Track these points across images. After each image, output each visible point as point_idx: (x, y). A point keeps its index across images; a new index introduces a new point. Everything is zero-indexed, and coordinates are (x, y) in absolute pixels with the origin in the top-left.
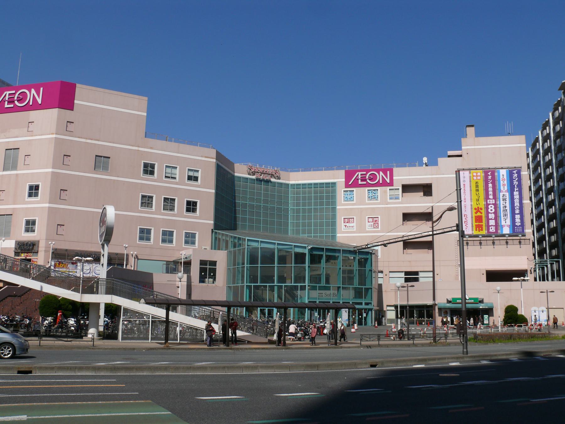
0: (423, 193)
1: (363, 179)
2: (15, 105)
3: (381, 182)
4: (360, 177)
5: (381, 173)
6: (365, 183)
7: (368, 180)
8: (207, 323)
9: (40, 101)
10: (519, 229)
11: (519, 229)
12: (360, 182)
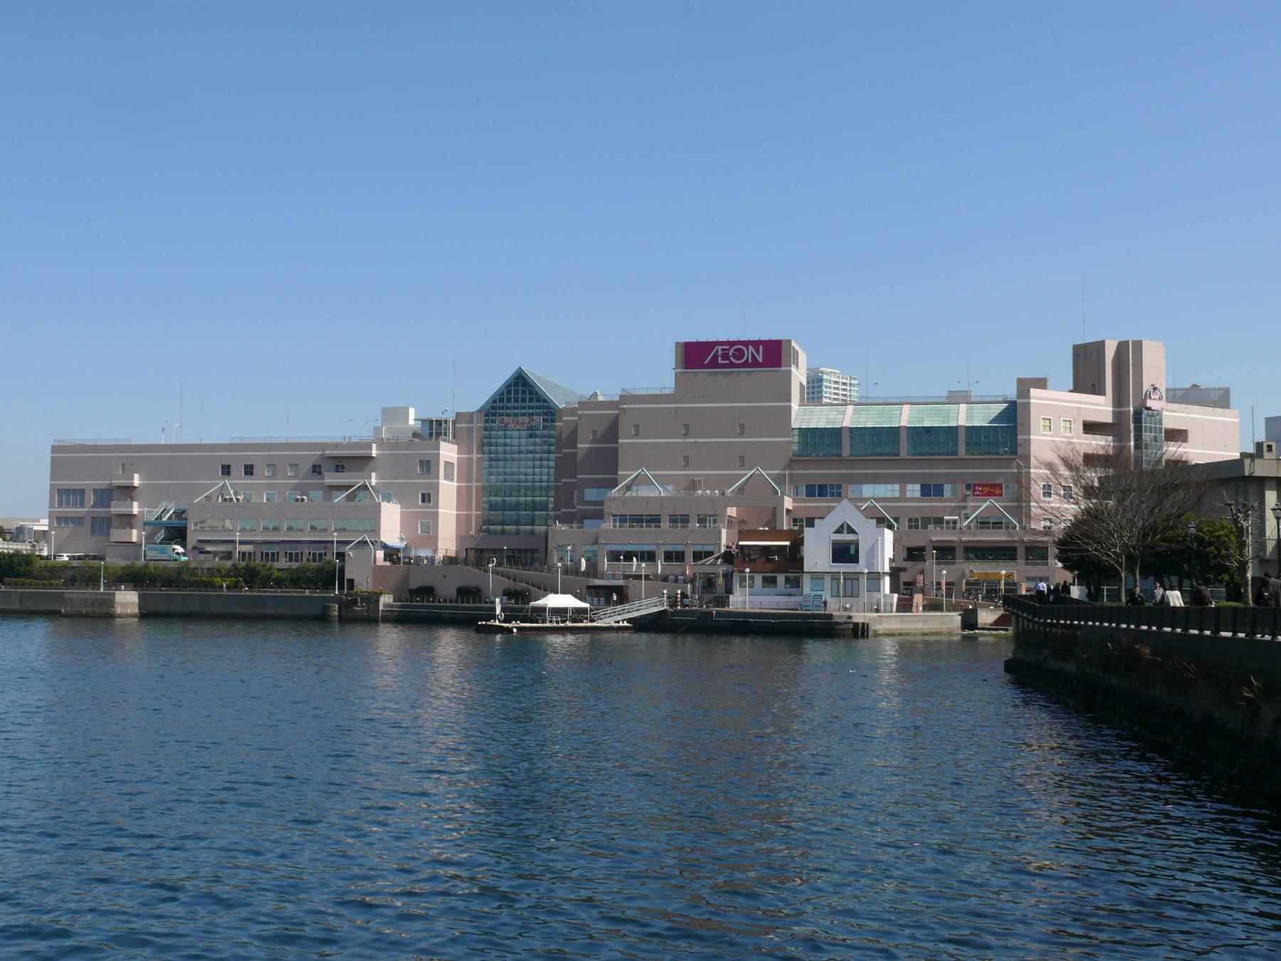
0: (1275, 492)
1: (725, 357)
3: (750, 361)
4: (720, 353)
5: (751, 348)
6: (728, 362)
7: (732, 358)
8: (735, 516)
9: (760, 359)
10: (537, 478)
11: (537, 478)
12: (720, 361)
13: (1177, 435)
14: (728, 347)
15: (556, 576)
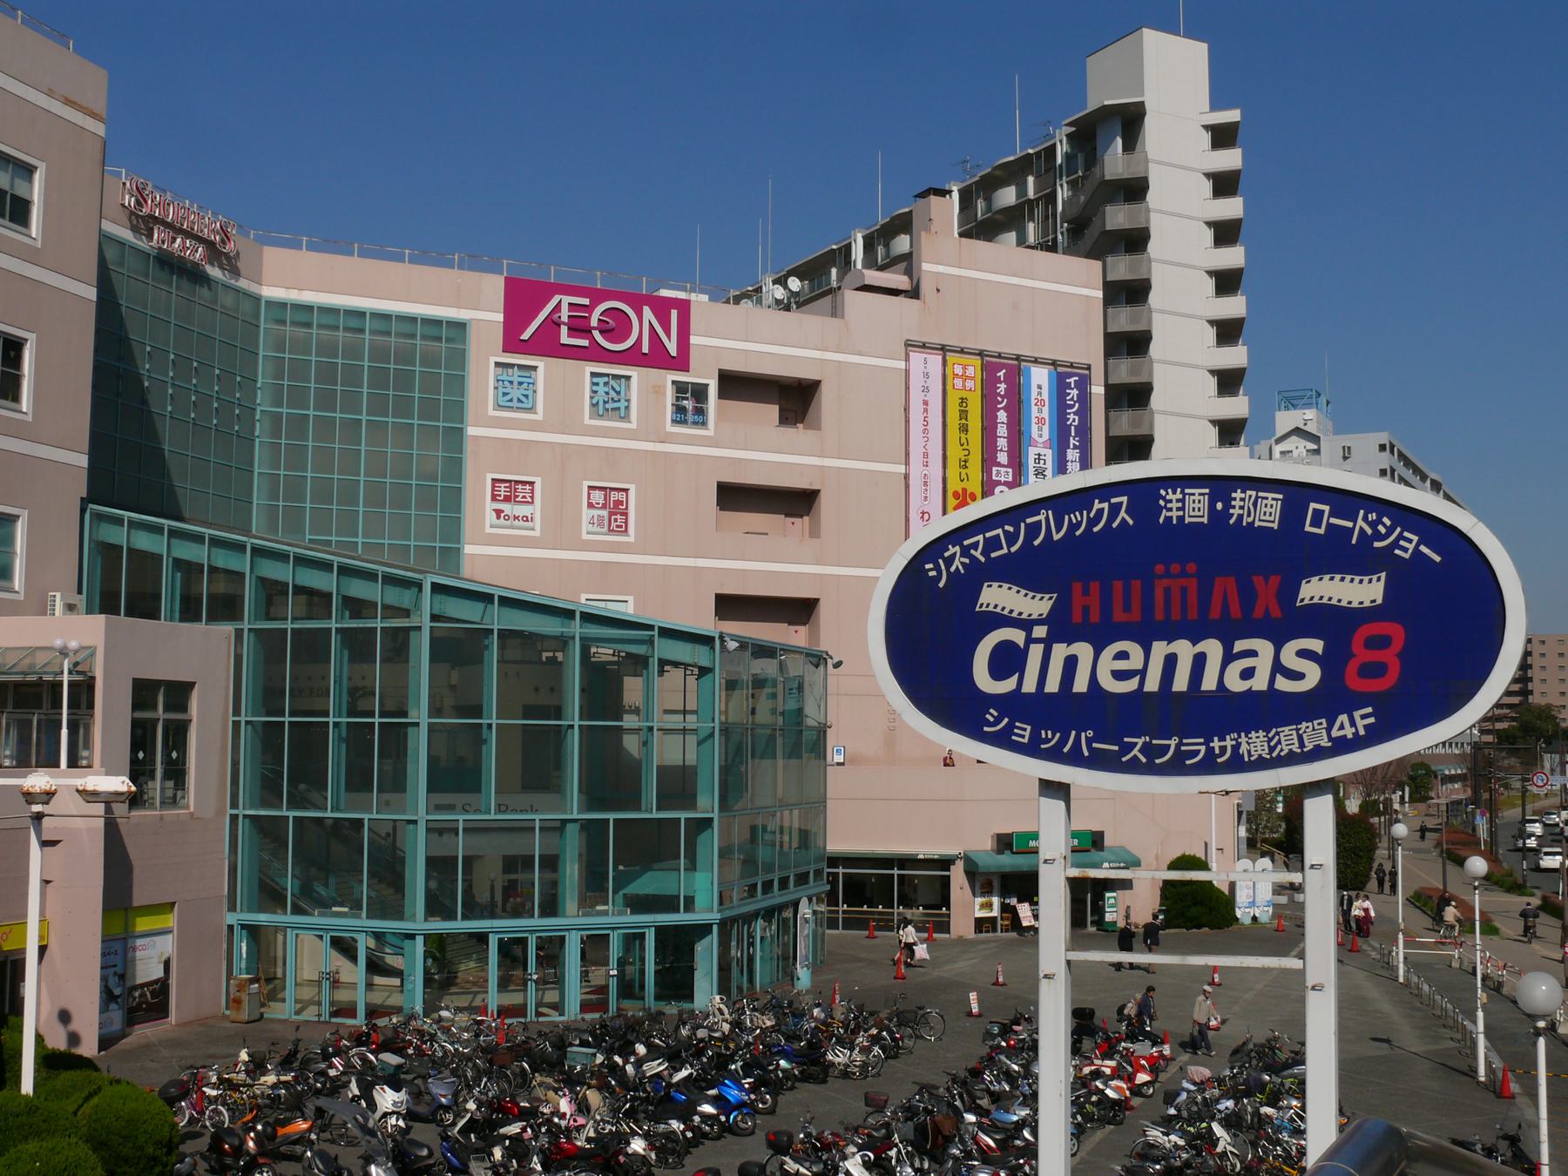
1: (579, 327)
2: (593, 340)
3: (645, 349)
4: (565, 314)
5: (647, 312)
6: (585, 343)
7: (596, 334)
12: (565, 338)
13: (19, 1104)
14: (586, 301)
15: (373, 894)
